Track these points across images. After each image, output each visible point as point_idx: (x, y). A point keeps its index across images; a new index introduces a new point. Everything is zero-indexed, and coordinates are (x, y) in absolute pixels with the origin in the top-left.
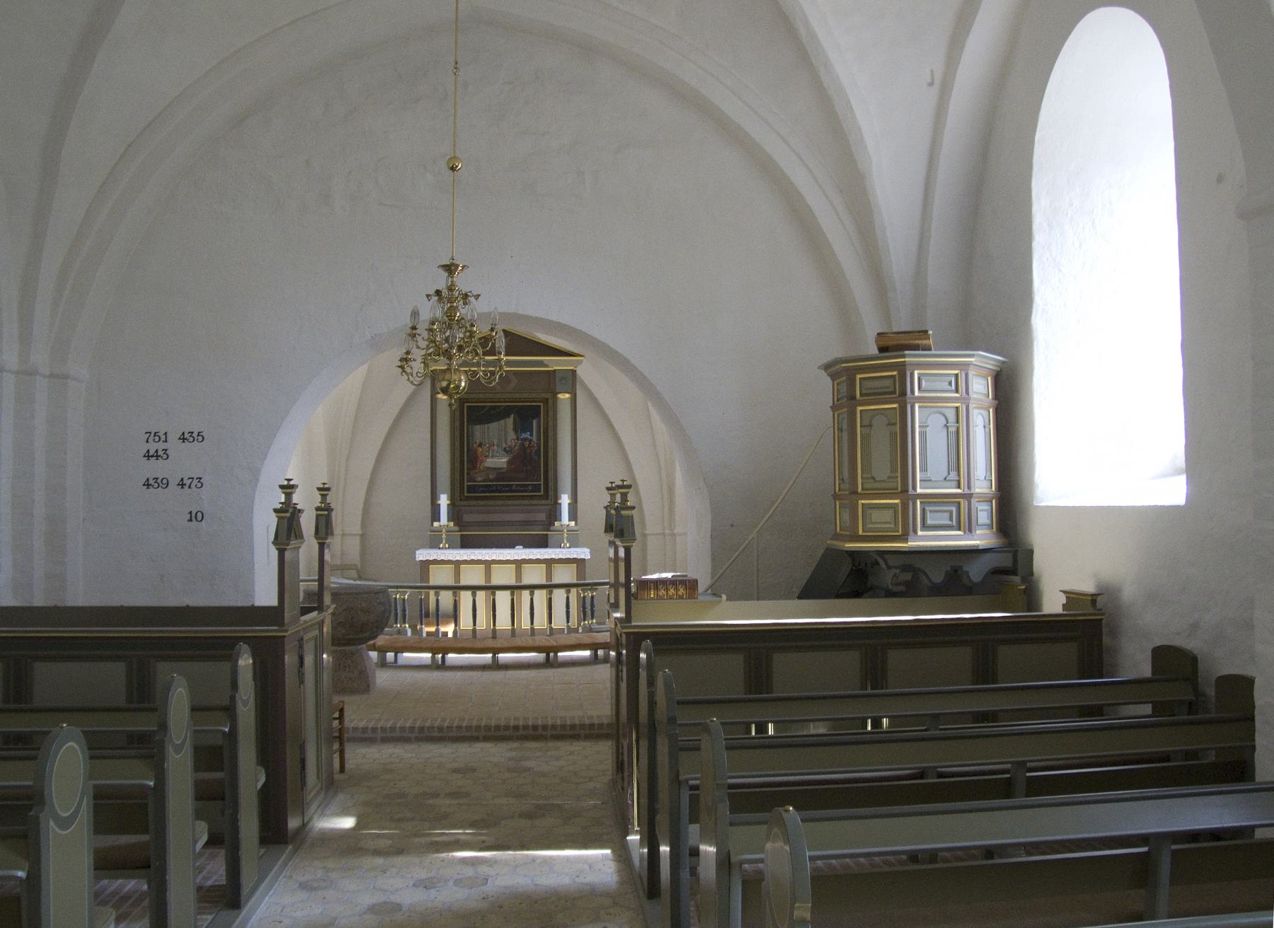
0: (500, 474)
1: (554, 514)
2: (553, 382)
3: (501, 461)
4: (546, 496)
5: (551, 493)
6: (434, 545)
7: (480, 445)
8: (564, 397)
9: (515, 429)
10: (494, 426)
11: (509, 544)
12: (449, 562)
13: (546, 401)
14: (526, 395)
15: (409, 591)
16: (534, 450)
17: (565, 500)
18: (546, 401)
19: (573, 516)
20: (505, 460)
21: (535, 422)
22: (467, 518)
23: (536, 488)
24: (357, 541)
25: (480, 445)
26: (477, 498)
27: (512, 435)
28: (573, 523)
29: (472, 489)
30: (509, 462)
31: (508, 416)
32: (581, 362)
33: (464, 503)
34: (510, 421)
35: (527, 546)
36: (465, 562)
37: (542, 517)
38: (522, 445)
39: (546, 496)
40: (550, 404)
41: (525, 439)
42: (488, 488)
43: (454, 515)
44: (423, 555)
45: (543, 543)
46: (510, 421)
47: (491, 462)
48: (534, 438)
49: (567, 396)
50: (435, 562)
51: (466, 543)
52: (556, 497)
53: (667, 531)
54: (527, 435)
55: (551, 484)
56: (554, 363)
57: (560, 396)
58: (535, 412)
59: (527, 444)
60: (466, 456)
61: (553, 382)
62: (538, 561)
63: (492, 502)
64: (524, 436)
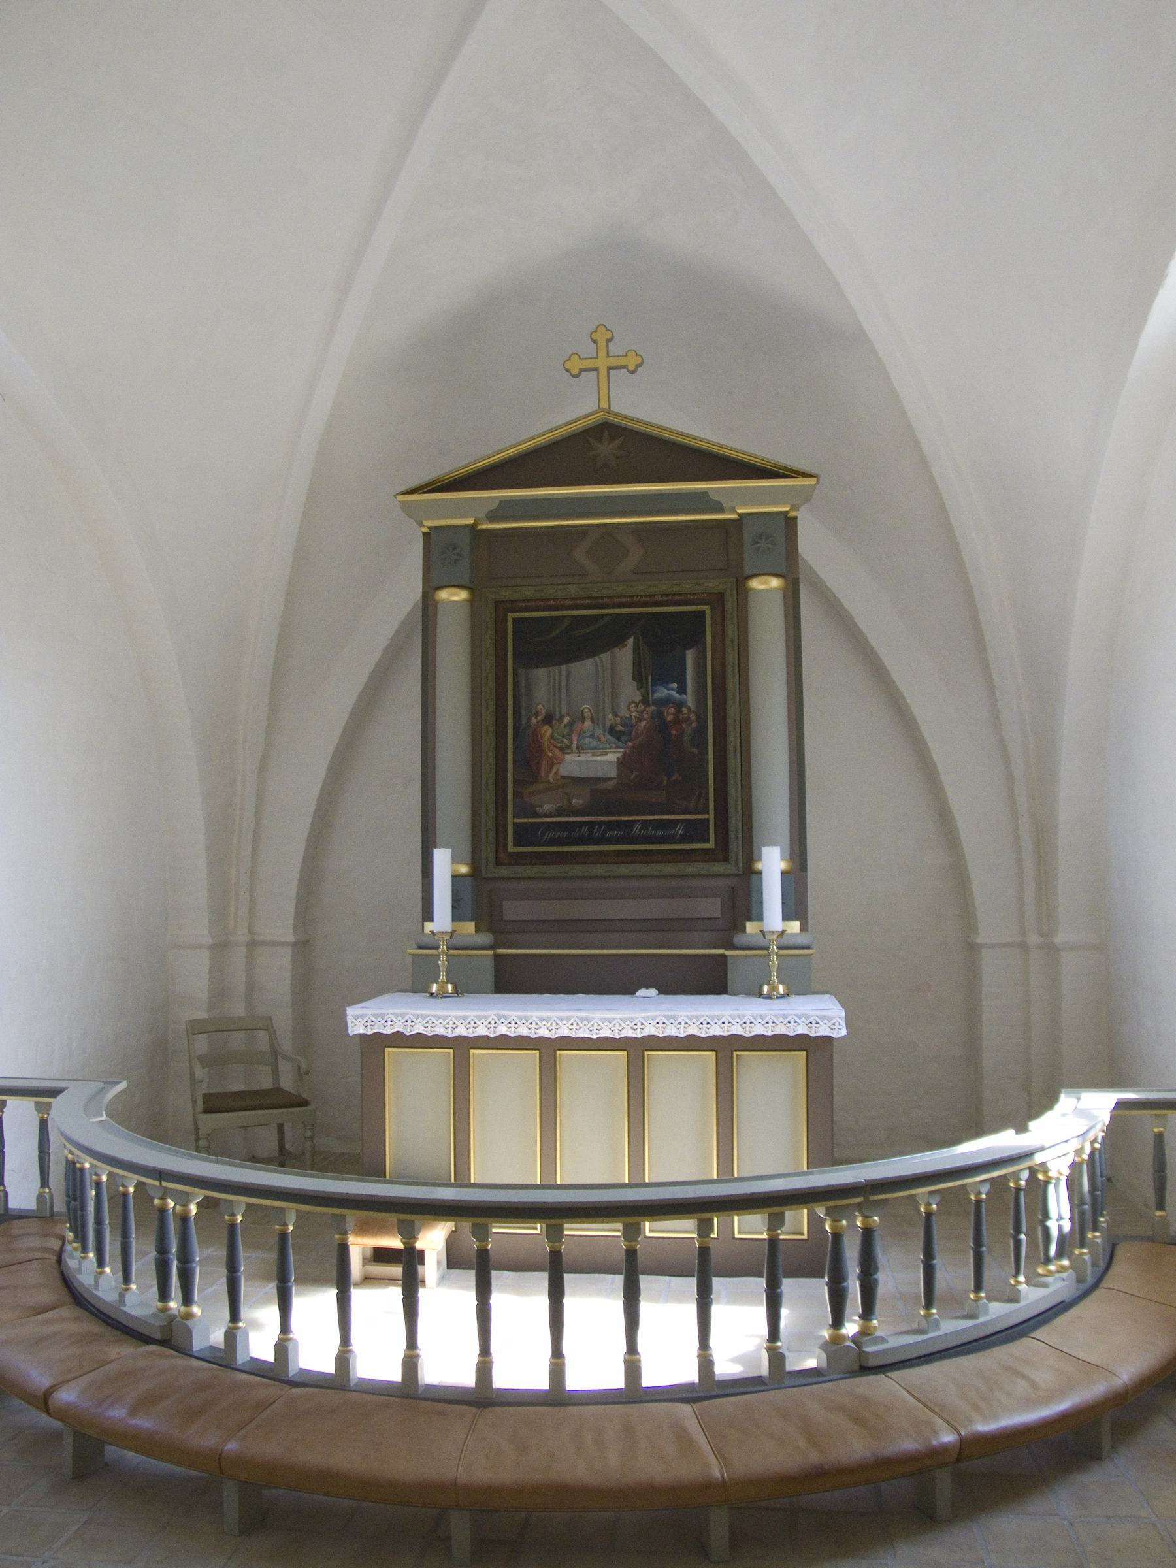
0: (601, 796)
1: (743, 902)
2: (737, 548)
3: (601, 761)
4: (722, 852)
5: (735, 846)
6: (418, 983)
7: (549, 719)
8: (767, 585)
9: (638, 677)
10: (583, 669)
11: (616, 981)
12: (438, 1041)
13: (717, 601)
14: (663, 587)
15: (200, 1194)
16: (688, 731)
17: (772, 863)
18: (717, 601)
19: (795, 907)
20: (612, 757)
21: (690, 656)
22: (514, 910)
23: (697, 831)
24: (285, 958)
25: (549, 719)
26: (541, 859)
27: (629, 691)
28: (795, 926)
29: (524, 835)
30: (622, 763)
31: (619, 642)
32: (806, 496)
33: (504, 871)
34: (625, 655)
35: (668, 988)
36: (484, 1042)
37: (711, 908)
38: (659, 715)
39: (722, 852)
40: (731, 607)
41: (666, 701)
42: (569, 833)
43: (474, 898)
44: (363, 1019)
45: (712, 980)
46: (625, 655)
47: (574, 764)
48: (690, 699)
49: (775, 582)
50: (399, 1040)
51: (510, 980)
52: (750, 856)
53: (1033, 939)
54: (668, 691)
55: (735, 821)
56: (740, 499)
57: (756, 584)
58: (688, 630)
59: (669, 713)
60: (510, 751)
61: (737, 548)
62: (692, 1043)
63: (576, 870)
64: (662, 692)
